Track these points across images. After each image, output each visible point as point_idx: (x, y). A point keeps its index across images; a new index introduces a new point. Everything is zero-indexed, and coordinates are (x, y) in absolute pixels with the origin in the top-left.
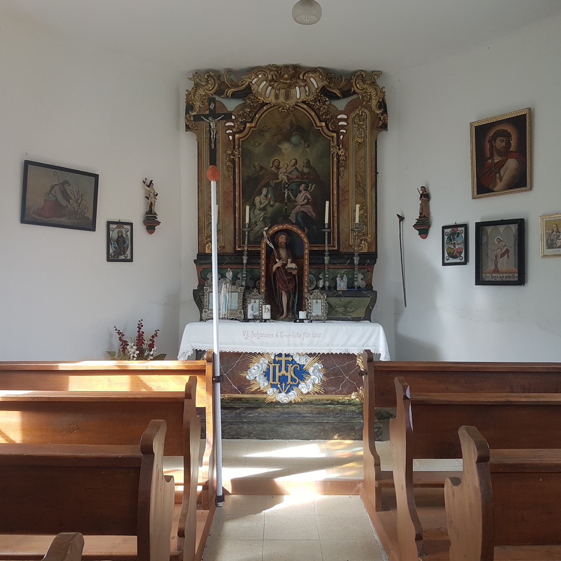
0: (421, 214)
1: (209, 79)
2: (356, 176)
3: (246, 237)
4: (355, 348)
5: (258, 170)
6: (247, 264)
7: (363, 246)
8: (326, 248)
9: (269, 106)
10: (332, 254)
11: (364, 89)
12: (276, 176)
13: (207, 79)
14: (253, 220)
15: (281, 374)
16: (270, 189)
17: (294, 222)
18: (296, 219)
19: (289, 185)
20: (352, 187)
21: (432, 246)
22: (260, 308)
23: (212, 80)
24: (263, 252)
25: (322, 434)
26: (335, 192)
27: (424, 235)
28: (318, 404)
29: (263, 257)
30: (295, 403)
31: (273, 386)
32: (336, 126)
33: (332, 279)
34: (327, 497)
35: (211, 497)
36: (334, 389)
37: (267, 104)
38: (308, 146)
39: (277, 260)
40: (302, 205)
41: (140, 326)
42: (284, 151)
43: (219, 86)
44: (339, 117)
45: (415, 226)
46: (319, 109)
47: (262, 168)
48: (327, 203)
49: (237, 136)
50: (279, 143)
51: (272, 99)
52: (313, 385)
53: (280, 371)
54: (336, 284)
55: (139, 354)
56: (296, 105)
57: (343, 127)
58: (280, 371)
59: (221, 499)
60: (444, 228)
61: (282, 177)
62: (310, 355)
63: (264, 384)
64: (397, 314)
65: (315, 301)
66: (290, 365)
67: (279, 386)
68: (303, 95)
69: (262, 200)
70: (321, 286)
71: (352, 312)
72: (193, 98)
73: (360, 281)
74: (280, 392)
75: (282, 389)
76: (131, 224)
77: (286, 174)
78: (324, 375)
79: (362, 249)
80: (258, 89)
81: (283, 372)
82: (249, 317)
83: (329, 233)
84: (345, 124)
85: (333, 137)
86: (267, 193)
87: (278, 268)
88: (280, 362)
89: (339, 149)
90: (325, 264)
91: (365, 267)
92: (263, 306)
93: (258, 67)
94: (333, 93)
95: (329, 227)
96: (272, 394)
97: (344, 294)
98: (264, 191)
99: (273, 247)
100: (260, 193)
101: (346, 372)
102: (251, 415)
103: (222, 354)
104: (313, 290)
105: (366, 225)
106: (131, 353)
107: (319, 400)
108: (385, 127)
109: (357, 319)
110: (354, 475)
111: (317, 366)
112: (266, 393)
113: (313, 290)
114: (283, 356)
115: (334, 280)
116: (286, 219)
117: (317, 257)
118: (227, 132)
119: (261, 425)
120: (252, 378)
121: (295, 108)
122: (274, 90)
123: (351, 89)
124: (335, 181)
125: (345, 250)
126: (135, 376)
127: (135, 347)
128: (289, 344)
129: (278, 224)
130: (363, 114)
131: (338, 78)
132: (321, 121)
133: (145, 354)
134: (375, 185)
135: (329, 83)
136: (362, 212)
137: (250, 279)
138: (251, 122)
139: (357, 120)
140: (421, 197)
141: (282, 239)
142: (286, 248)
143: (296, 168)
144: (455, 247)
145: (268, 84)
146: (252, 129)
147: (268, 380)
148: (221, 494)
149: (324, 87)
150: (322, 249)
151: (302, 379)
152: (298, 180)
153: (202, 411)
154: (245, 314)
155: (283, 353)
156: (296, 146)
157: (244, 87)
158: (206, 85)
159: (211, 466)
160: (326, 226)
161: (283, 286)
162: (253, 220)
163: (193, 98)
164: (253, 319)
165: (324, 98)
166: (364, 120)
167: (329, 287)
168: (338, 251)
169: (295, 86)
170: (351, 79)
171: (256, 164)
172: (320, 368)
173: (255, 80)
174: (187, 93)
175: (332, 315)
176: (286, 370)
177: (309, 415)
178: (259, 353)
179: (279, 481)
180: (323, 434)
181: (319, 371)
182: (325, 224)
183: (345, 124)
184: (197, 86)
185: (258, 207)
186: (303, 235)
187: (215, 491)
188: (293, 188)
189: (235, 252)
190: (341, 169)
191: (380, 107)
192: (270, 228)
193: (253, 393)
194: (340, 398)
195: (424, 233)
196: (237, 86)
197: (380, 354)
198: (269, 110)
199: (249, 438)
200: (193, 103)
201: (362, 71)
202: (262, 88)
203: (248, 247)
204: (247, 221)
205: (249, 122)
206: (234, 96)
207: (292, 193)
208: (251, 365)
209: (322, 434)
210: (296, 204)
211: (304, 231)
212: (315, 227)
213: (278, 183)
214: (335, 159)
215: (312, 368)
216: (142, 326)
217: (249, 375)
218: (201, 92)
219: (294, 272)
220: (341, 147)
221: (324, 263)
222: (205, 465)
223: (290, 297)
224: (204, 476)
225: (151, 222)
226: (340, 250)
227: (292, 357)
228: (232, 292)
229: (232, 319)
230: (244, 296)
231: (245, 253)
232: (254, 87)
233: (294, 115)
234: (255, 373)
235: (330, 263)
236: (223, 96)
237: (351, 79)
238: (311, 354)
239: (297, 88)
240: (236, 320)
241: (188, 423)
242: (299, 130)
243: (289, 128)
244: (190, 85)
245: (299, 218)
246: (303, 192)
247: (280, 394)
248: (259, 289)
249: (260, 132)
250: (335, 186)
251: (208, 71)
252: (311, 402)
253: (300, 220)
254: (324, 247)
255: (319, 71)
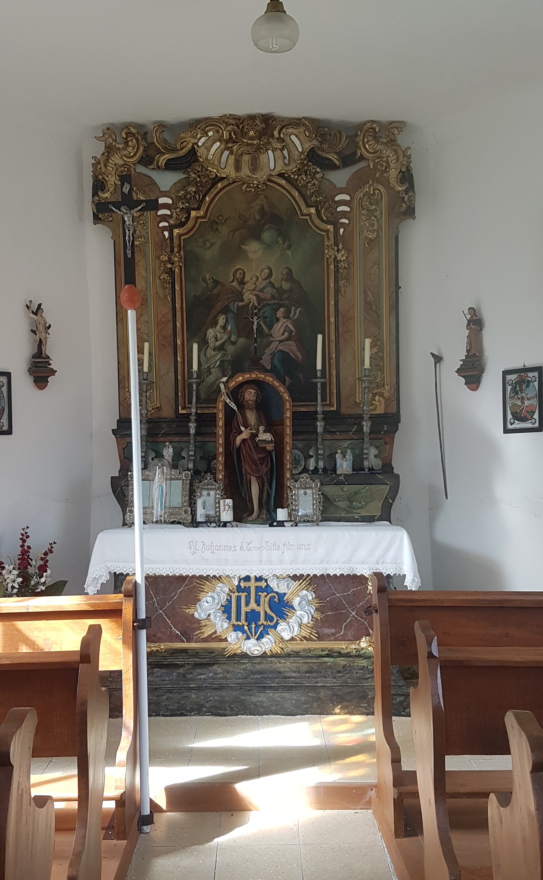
0: (468, 351)
1: (129, 139)
2: (365, 293)
3: (194, 393)
4: (364, 566)
5: (210, 286)
6: (197, 434)
7: (377, 403)
8: (319, 409)
9: (226, 182)
10: (328, 416)
11: (377, 152)
12: (240, 296)
13: (126, 139)
14: (205, 366)
15: (248, 609)
16: (230, 315)
17: (269, 368)
18: (272, 363)
19: (259, 310)
20: (359, 311)
21: (487, 403)
22: (216, 503)
23: (134, 141)
24: (221, 416)
25: (315, 705)
26: (332, 320)
27: (475, 386)
28: (308, 657)
29: (221, 424)
30: (272, 656)
31: (236, 628)
32: (332, 214)
33: (328, 456)
34: (320, 813)
35: (131, 818)
36: (333, 631)
37: (223, 178)
38: (289, 247)
39: (242, 428)
40: (281, 342)
41: (24, 538)
42: (251, 255)
43: (144, 150)
44: (337, 198)
45: (459, 371)
46: (305, 186)
47: (216, 283)
48: (320, 337)
49: (176, 231)
50: (243, 241)
51: (230, 171)
52: (300, 626)
53: (247, 603)
54: (336, 465)
55: (22, 582)
56: (269, 180)
57: (344, 214)
58: (247, 604)
59: (148, 820)
60: (506, 373)
61: (249, 297)
62: (295, 578)
63: (222, 626)
64: (434, 510)
65: (302, 492)
66: (263, 595)
67: (246, 628)
68: (280, 163)
69: (219, 335)
70: (312, 468)
71: (361, 507)
72: (103, 170)
73: (372, 459)
74: (248, 638)
75: (251, 633)
76: (8, 375)
77: (254, 292)
78: (317, 609)
79: (375, 409)
80: (207, 155)
81: (253, 605)
82: (199, 519)
83: (324, 385)
84: (348, 209)
85: (327, 231)
86: (226, 324)
87: (244, 440)
88: (247, 590)
89: (338, 251)
90: (317, 433)
91: (380, 436)
92: (222, 501)
93: (206, 119)
94: (329, 159)
95: (323, 376)
96: (237, 642)
97: (348, 480)
98: (221, 320)
99: (235, 408)
100: (214, 323)
101: (352, 604)
102: (202, 677)
103: (152, 581)
104: (300, 474)
105: (382, 370)
106: (8, 581)
107: (310, 650)
108: (410, 212)
109: (369, 519)
110: (363, 777)
111: (306, 596)
112: (226, 640)
113: (300, 474)
114: (253, 580)
115: (332, 457)
116: (256, 365)
117: (304, 422)
118: (161, 225)
119: (218, 693)
120: (203, 616)
121: (266, 185)
122: (233, 156)
123: (356, 151)
124: (332, 303)
125: (349, 411)
126: (8, 623)
127: (16, 572)
128: (261, 561)
129: (243, 371)
130: (376, 192)
131: (336, 135)
132: (308, 206)
133: (33, 583)
134: (395, 307)
135: (321, 143)
136: (375, 350)
137: (200, 458)
138: (198, 209)
139: (366, 203)
140: (468, 324)
141: (250, 395)
142: (257, 409)
143: (270, 282)
144: (523, 403)
145: (223, 146)
146: (200, 220)
147: (229, 618)
148: (148, 813)
149: (312, 150)
150: (312, 409)
151: (282, 616)
152: (275, 301)
153: (115, 677)
154: (194, 514)
155: (252, 576)
156: (269, 246)
157: (185, 151)
158: (124, 149)
159: (131, 766)
160: (319, 374)
161: (251, 469)
162: (205, 366)
163: (103, 170)
164: (206, 522)
165: (313, 168)
166: (378, 202)
167: (325, 470)
168: (338, 412)
169: (267, 150)
170: (357, 135)
171: (208, 276)
172: (310, 598)
173: (203, 140)
174: (93, 161)
175: (329, 513)
176: (258, 603)
177: (294, 675)
178: (215, 576)
179: (242, 788)
180: (316, 705)
181: (309, 603)
182: (316, 371)
183: (348, 209)
184: (110, 150)
185: (212, 345)
186: (282, 389)
187: (138, 808)
188: (266, 314)
189: (177, 417)
190: (341, 283)
191: (402, 181)
192: (231, 378)
193: (205, 640)
194: (342, 646)
195: (473, 383)
196: (174, 150)
197: (405, 575)
198: (226, 189)
199: (199, 714)
200: (103, 178)
201: (373, 122)
202: (212, 151)
203: (197, 408)
204: (195, 367)
205: (194, 209)
206: (170, 166)
207: (265, 323)
208: (202, 595)
209: (315, 705)
210: (271, 339)
211: (283, 382)
212: (301, 375)
213: (243, 306)
214: (332, 267)
215: (298, 598)
216: (28, 537)
217: (199, 611)
218: (117, 160)
219: (270, 447)
220: (340, 246)
221: (316, 432)
222: (120, 765)
223: (263, 486)
224: (119, 784)
225: (41, 371)
226: (342, 410)
227: (266, 581)
228: (171, 479)
229: (172, 523)
230: (191, 485)
231: (193, 418)
232: (201, 152)
233: (266, 197)
234: (208, 609)
235: (326, 431)
236: (152, 167)
237: (357, 135)
238: (295, 576)
239: (270, 152)
240: (179, 523)
241: (85, 704)
242: (273, 220)
243: (257, 217)
244: (99, 149)
245: (276, 362)
246: (282, 320)
247: (248, 641)
248: (214, 474)
249: (213, 225)
250: (332, 309)
251: (127, 126)
252: (297, 654)
253: (278, 365)
254: (316, 405)
255: (304, 125)
